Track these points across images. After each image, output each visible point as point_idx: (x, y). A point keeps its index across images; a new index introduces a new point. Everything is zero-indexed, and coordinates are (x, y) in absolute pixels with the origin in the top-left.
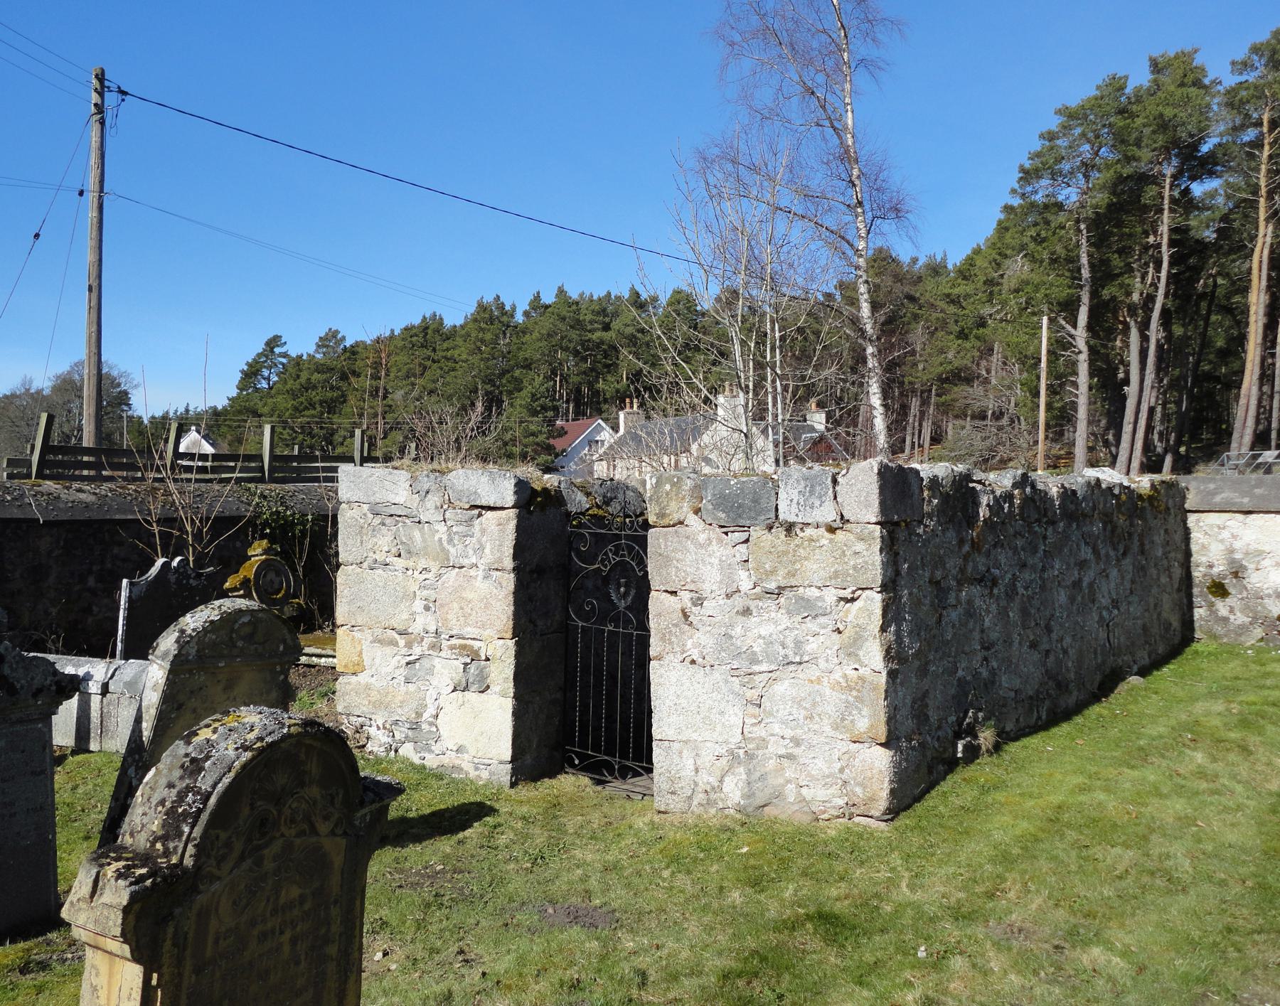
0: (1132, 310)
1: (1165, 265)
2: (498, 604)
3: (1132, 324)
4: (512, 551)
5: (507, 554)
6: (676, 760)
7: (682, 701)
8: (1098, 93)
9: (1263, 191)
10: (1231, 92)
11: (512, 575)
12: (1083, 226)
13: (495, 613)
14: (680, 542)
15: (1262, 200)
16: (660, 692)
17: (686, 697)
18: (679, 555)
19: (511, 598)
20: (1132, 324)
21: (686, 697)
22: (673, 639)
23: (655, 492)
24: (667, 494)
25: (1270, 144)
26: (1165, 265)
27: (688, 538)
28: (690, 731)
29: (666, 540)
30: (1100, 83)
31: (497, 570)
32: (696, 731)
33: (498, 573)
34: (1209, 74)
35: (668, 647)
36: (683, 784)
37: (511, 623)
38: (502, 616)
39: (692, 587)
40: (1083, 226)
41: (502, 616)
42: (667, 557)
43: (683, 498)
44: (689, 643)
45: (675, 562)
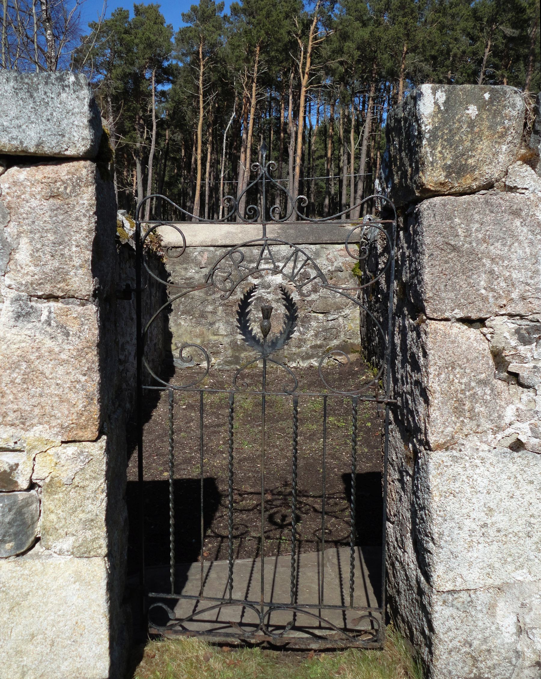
0: (137, 152)
1: (154, 128)
2: (61, 370)
3: (137, 161)
4: (88, 255)
5: (77, 262)
6: (482, 620)
7: (497, 517)
8: (113, 18)
9: (201, 92)
10: (183, 32)
11: (92, 308)
12: (109, 100)
13: (53, 390)
14: (497, 223)
15: (201, 96)
16: (452, 505)
17: (506, 511)
18: (496, 249)
19: (93, 356)
20: (137, 161)
21: (506, 511)
22: (479, 408)
23: (445, 122)
24: (472, 124)
25: (204, 65)
26: (154, 128)
27: (516, 213)
28: (510, 568)
29: (469, 220)
30: (114, 12)
31: (50, 297)
32: (521, 567)
33: (53, 304)
34: (166, 21)
35: (470, 425)
36: (495, 659)
37: (95, 409)
38: (72, 396)
39: (520, 308)
40: (109, 100)
41: (72, 396)
42: (472, 252)
43: (503, 136)
44: (509, 413)
45: (487, 262)
